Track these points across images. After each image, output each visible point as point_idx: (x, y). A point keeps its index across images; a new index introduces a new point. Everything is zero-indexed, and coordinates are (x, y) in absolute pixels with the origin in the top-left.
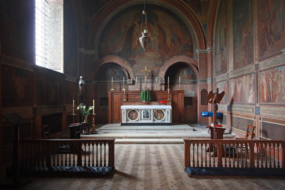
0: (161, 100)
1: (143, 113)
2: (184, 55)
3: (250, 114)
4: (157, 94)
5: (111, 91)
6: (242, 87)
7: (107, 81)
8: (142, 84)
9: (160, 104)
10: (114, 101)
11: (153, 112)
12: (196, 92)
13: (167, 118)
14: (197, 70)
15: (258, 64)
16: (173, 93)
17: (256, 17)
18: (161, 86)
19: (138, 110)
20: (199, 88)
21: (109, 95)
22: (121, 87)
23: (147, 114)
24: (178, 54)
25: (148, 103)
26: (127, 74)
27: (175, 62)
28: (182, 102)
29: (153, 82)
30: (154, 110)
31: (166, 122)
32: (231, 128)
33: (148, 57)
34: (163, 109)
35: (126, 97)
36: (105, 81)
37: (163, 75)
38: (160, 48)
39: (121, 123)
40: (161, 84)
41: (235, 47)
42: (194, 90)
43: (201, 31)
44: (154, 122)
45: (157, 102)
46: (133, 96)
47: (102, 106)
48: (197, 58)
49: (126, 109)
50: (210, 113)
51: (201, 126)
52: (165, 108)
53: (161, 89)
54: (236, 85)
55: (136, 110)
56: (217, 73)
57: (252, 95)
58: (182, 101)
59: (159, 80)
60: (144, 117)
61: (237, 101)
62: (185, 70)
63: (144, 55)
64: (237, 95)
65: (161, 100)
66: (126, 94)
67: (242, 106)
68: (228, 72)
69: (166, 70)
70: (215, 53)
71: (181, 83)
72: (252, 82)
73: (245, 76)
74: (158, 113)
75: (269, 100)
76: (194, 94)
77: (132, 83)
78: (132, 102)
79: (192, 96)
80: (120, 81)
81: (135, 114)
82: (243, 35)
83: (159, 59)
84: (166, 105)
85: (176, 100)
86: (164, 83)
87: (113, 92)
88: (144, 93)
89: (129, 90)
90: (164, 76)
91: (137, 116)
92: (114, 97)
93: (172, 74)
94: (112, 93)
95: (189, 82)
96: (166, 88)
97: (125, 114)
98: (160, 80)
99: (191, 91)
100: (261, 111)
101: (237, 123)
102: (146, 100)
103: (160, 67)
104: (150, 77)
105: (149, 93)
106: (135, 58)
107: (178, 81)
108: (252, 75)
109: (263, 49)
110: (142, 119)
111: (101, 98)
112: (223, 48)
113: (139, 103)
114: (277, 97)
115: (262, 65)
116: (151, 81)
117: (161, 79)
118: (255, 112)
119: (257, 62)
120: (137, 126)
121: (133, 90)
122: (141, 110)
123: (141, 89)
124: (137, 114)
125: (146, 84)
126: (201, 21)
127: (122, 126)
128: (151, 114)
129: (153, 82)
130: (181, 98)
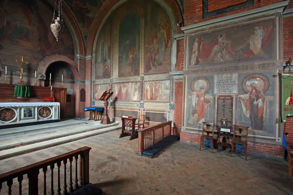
1: (24, 112)
2: (67, 56)
3: (135, 107)
6: (127, 90)
11: (38, 109)
13: (54, 114)
15: (143, 77)
17: (143, 47)
18: (40, 82)
19: (16, 108)
24: (60, 53)
27: (57, 60)
28: (64, 99)
30: (38, 107)
31: (53, 118)
32: (114, 118)
33: (23, 46)
34: (51, 105)
38: (39, 40)
40: (40, 80)
41: (120, 62)
43: (82, 40)
44: (39, 120)
48: (77, 61)
50: (97, 108)
52: (53, 105)
53: (40, 85)
54: (121, 88)
55: (12, 109)
56: (97, 77)
57: (137, 96)
60: (25, 116)
61: (121, 99)
62: (65, 70)
63: (17, 42)
64: (122, 95)
67: (127, 102)
68: (111, 78)
70: (96, 62)
72: (137, 87)
73: (131, 83)
74: (43, 110)
75: (151, 99)
79: (70, 94)
82: (129, 56)
86: (45, 79)
91: (13, 115)
93: (54, 69)
96: (47, 85)
100: (145, 106)
101: (121, 114)
105: (28, 88)
108: (137, 83)
109: (148, 69)
110: (22, 118)
112: (105, 59)
113: (11, 100)
114: (159, 97)
115: (147, 78)
116: (27, 75)
118: (140, 106)
119: (142, 76)
124: (15, 114)
125: (22, 77)
126: (83, 32)
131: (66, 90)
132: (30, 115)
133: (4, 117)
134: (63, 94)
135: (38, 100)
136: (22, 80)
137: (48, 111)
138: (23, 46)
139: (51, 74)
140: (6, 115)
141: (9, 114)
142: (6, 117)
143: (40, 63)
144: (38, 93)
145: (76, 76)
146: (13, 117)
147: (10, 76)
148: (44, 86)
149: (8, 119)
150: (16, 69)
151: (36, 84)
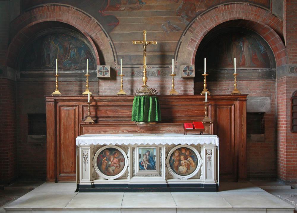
0: (185, 119)
1: (140, 158)
4: (174, 103)
5: (55, 96)
7: (47, 72)
8: (135, 79)
9: (186, 132)
10: (62, 124)
11: (167, 153)
12: (273, 101)
13: (207, 170)
14: (281, 42)
16: (217, 102)
18: (185, 85)
19: (125, 148)
20: (284, 88)
21: (47, 108)
22: (81, 86)
23: (151, 159)
25: (152, 128)
26: (96, 51)
28: (241, 126)
29: (163, 73)
30: (169, 148)
31: (202, 181)
33: (150, 7)
34: (196, 144)
35: (93, 113)
36: (42, 72)
37: (189, 54)
39: (78, 186)
40: (186, 79)
42: (270, 96)
44: (170, 182)
45: (177, 125)
46: (111, 110)
47: (33, 136)
48: (280, 9)
49: (91, 146)
51: (292, 188)
52: (201, 143)
53: (185, 91)
58: (241, 122)
59: (179, 69)
60: (141, 167)
62: (246, 44)
65: (185, 119)
66: (94, 103)
69: (198, 41)
71: (239, 78)
74: (179, 156)
76: (269, 105)
77: (108, 75)
78: (108, 125)
79: (263, 110)
80: (79, 72)
81: (116, 160)
83: (179, 14)
84: (201, 133)
85: (224, 121)
86: (193, 75)
87: (57, 98)
88: (140, 100)
89: (101, 94)
90: (192, 57)
91: (122, 163)
92: (62, 112)
93: (214, 51)
94: (56, 102)
95: (257, 74)
96: (198, 90)
97: (89, 159)
98: (183, 67)
99: (261, 98)
102: (145, 121)
103: (183, 34)
104: (157, 61)
105: (153, 101)
106: (117, 9)
107: (226, 72)
110: (136, 173)
111: (30, 116)
113: (128, 128)
116: (158, 71)
117: (184, 64)
120: (122, 193)
121: (113, 94)
122: (134, 149)
123: (132, 91)
124: (123, 160)
125: (146, 77)
127: (79, 194)
128: (160, 159)
129: (163, 73)
130: (238, 115)
131: (246, 100)
132: (151, 168)
133: (106, 167)
134: (238, 111)
135: (176, 128)
136: (146, 83)
137: (191, 159)
138: (150, 7)
139: (205, 59)
140: (110, 163)
141: (115, 161)
142: (110, 166)
143: (183, 39)
144: (180, 112)
145: (279, 56)
146: (121, 166)
147: (130, 78)
148: (192, 93)
149: (113, 170)
150: (139, 62)
151: (174, 90)
